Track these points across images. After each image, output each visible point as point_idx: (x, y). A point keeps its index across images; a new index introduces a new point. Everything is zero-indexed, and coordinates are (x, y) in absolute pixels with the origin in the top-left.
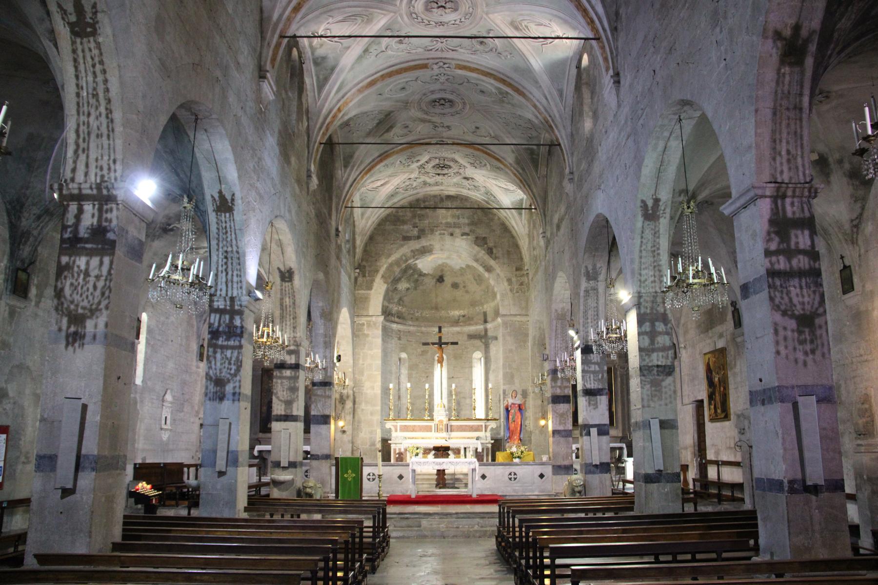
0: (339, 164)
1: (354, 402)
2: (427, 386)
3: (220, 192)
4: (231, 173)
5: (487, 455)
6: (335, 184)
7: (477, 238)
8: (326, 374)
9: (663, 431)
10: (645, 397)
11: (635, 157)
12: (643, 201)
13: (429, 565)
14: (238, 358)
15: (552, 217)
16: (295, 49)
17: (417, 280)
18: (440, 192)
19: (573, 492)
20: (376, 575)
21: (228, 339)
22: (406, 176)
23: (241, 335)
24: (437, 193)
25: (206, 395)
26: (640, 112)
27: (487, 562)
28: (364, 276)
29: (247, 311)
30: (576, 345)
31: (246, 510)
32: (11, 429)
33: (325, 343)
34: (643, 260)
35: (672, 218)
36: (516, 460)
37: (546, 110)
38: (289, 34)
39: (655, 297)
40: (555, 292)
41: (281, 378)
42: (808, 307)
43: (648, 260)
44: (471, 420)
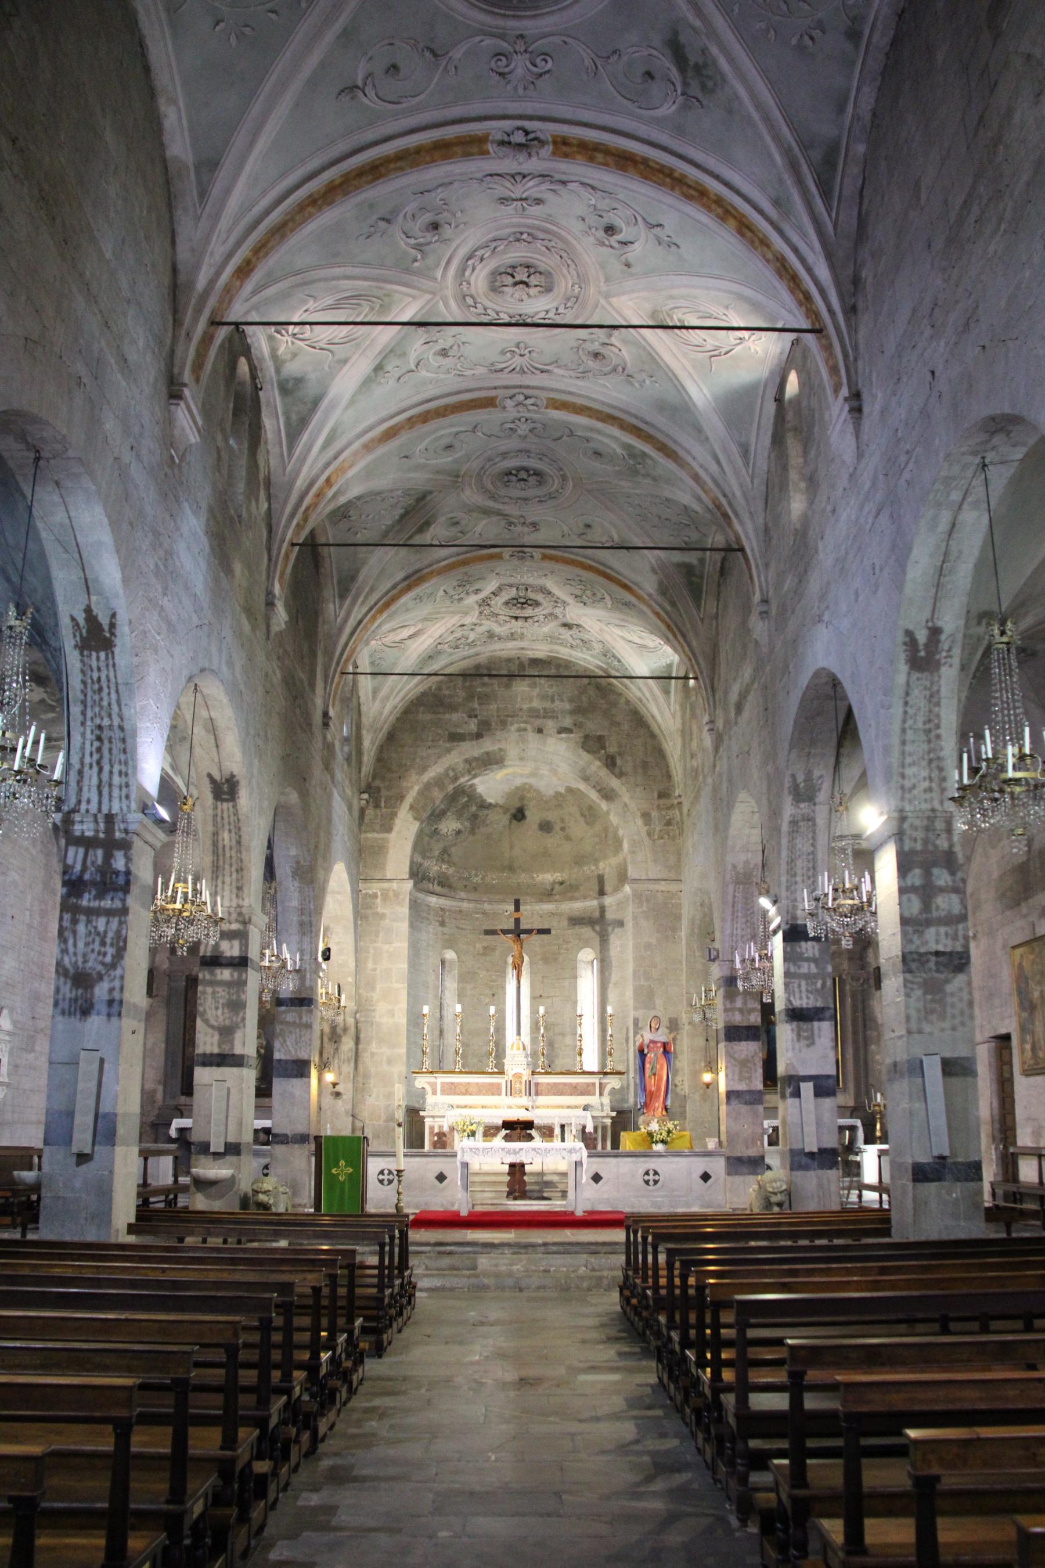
0: (330, 592)
1: (357, 1040)
2: (492, 1010)
3: (88, 610)
4: (109, 571)
5: (604, 1140)
6: (322, 629)
7: (586, 737)
8: (303, 979)
9: (948, 1079)
10: (914, 1014)
11: (893, 547)
12: (909, 633)
13: (490, 1341)
14: (118, 932)
15: (726, 693)
16: (243, 361)
17: (475, 817)
18: (519, 653)
19: (768, 1205)
20: (386, 1359)
21: (100, 896)
22: (455, 620)
23: (126, 888)
24: (513, 654)
25: (56, 1004)
26: (903, 458)
27: (603, 1337)
28: (377, 806)
29: (137, 843)
30: (772, 927)
31: (131, 1229)
33: (302, 924)
34: (909, 748)
35: (963, 668)
36: (659, 1147)
37: (718, 485)
38: (232, 318)
39: (931, 819)
40: (732, 832)
41: (212, 983)
43: (918, 747)
44: (575, 1073)
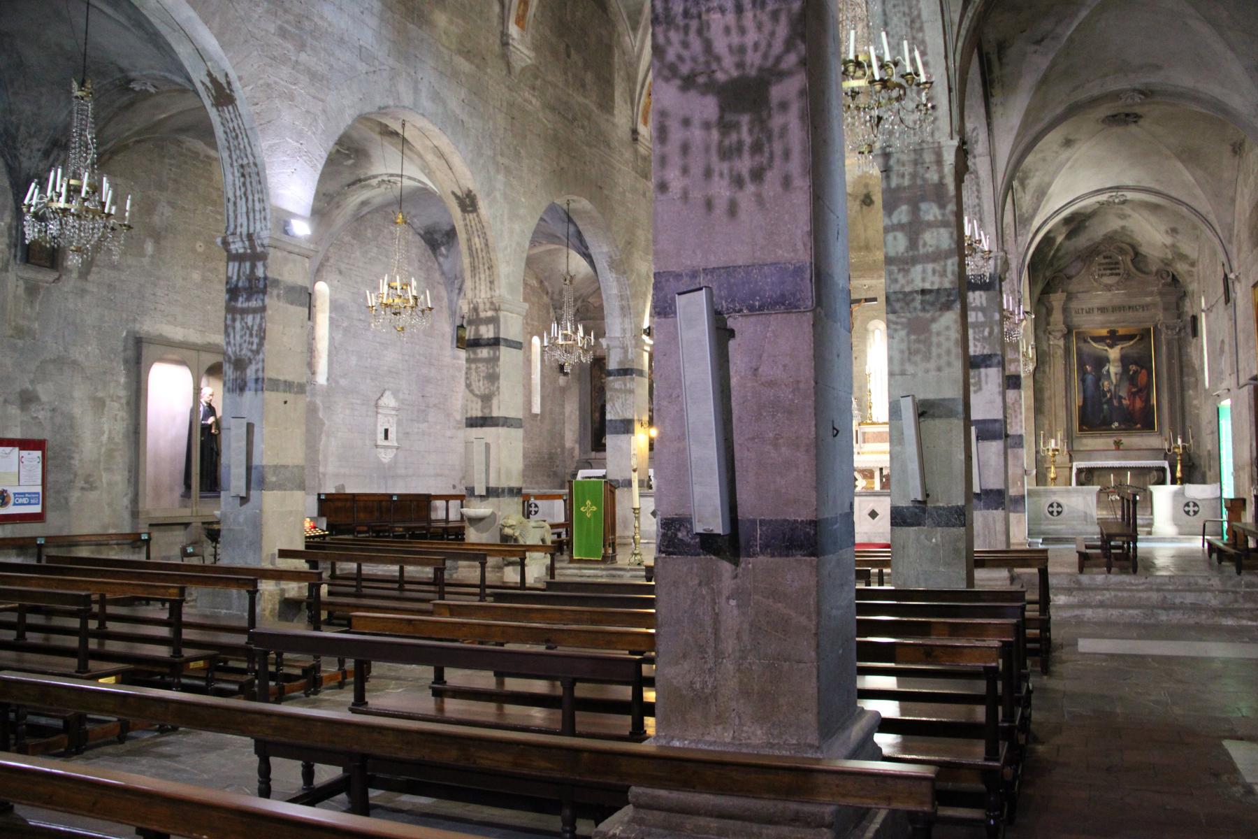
3: (209, 74)
4: (210, 42)
14: (260, 325)
21: (248, 299)
32: (49, 445)
33: (622, 308)
42: (753, 59)
